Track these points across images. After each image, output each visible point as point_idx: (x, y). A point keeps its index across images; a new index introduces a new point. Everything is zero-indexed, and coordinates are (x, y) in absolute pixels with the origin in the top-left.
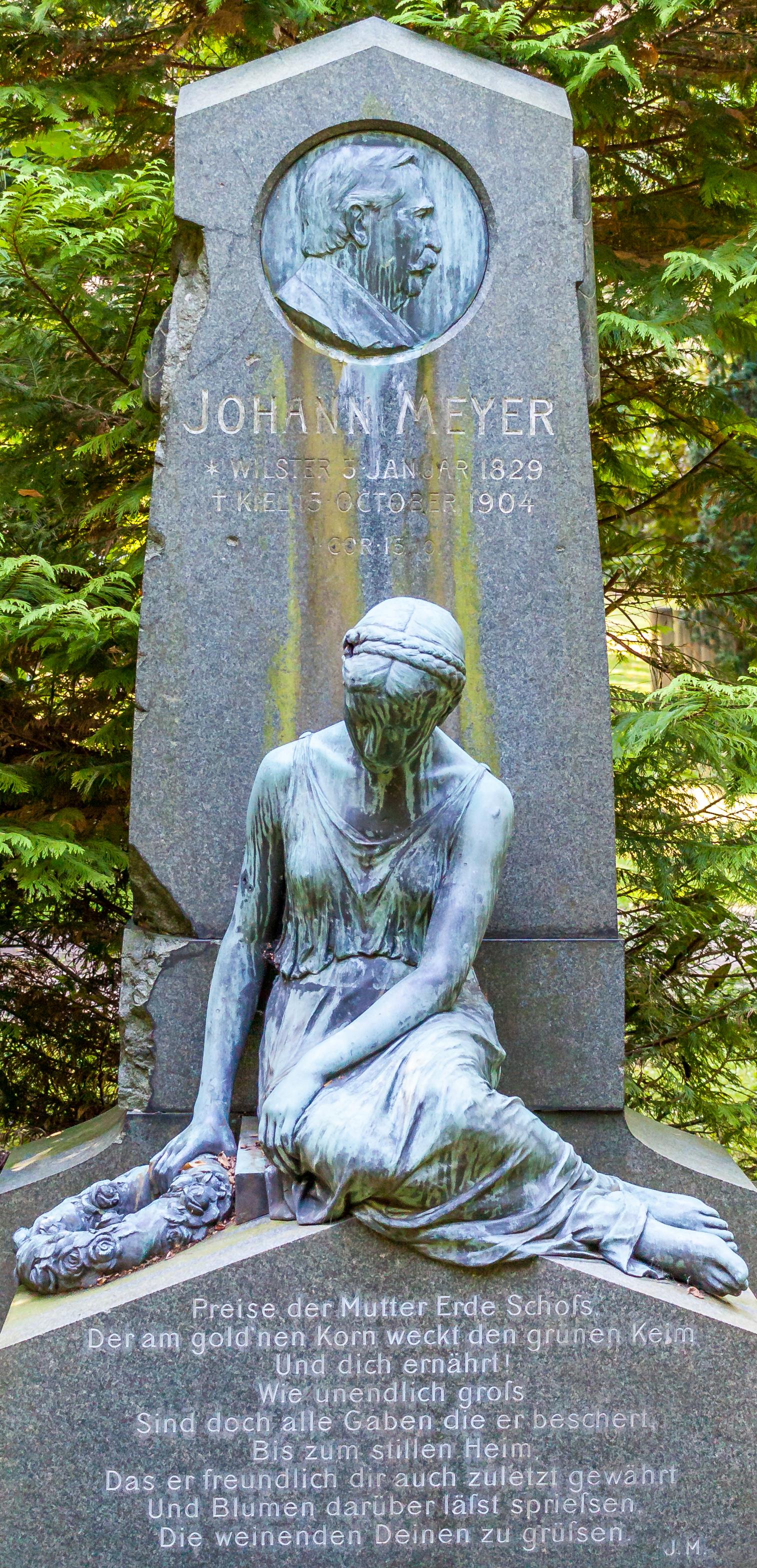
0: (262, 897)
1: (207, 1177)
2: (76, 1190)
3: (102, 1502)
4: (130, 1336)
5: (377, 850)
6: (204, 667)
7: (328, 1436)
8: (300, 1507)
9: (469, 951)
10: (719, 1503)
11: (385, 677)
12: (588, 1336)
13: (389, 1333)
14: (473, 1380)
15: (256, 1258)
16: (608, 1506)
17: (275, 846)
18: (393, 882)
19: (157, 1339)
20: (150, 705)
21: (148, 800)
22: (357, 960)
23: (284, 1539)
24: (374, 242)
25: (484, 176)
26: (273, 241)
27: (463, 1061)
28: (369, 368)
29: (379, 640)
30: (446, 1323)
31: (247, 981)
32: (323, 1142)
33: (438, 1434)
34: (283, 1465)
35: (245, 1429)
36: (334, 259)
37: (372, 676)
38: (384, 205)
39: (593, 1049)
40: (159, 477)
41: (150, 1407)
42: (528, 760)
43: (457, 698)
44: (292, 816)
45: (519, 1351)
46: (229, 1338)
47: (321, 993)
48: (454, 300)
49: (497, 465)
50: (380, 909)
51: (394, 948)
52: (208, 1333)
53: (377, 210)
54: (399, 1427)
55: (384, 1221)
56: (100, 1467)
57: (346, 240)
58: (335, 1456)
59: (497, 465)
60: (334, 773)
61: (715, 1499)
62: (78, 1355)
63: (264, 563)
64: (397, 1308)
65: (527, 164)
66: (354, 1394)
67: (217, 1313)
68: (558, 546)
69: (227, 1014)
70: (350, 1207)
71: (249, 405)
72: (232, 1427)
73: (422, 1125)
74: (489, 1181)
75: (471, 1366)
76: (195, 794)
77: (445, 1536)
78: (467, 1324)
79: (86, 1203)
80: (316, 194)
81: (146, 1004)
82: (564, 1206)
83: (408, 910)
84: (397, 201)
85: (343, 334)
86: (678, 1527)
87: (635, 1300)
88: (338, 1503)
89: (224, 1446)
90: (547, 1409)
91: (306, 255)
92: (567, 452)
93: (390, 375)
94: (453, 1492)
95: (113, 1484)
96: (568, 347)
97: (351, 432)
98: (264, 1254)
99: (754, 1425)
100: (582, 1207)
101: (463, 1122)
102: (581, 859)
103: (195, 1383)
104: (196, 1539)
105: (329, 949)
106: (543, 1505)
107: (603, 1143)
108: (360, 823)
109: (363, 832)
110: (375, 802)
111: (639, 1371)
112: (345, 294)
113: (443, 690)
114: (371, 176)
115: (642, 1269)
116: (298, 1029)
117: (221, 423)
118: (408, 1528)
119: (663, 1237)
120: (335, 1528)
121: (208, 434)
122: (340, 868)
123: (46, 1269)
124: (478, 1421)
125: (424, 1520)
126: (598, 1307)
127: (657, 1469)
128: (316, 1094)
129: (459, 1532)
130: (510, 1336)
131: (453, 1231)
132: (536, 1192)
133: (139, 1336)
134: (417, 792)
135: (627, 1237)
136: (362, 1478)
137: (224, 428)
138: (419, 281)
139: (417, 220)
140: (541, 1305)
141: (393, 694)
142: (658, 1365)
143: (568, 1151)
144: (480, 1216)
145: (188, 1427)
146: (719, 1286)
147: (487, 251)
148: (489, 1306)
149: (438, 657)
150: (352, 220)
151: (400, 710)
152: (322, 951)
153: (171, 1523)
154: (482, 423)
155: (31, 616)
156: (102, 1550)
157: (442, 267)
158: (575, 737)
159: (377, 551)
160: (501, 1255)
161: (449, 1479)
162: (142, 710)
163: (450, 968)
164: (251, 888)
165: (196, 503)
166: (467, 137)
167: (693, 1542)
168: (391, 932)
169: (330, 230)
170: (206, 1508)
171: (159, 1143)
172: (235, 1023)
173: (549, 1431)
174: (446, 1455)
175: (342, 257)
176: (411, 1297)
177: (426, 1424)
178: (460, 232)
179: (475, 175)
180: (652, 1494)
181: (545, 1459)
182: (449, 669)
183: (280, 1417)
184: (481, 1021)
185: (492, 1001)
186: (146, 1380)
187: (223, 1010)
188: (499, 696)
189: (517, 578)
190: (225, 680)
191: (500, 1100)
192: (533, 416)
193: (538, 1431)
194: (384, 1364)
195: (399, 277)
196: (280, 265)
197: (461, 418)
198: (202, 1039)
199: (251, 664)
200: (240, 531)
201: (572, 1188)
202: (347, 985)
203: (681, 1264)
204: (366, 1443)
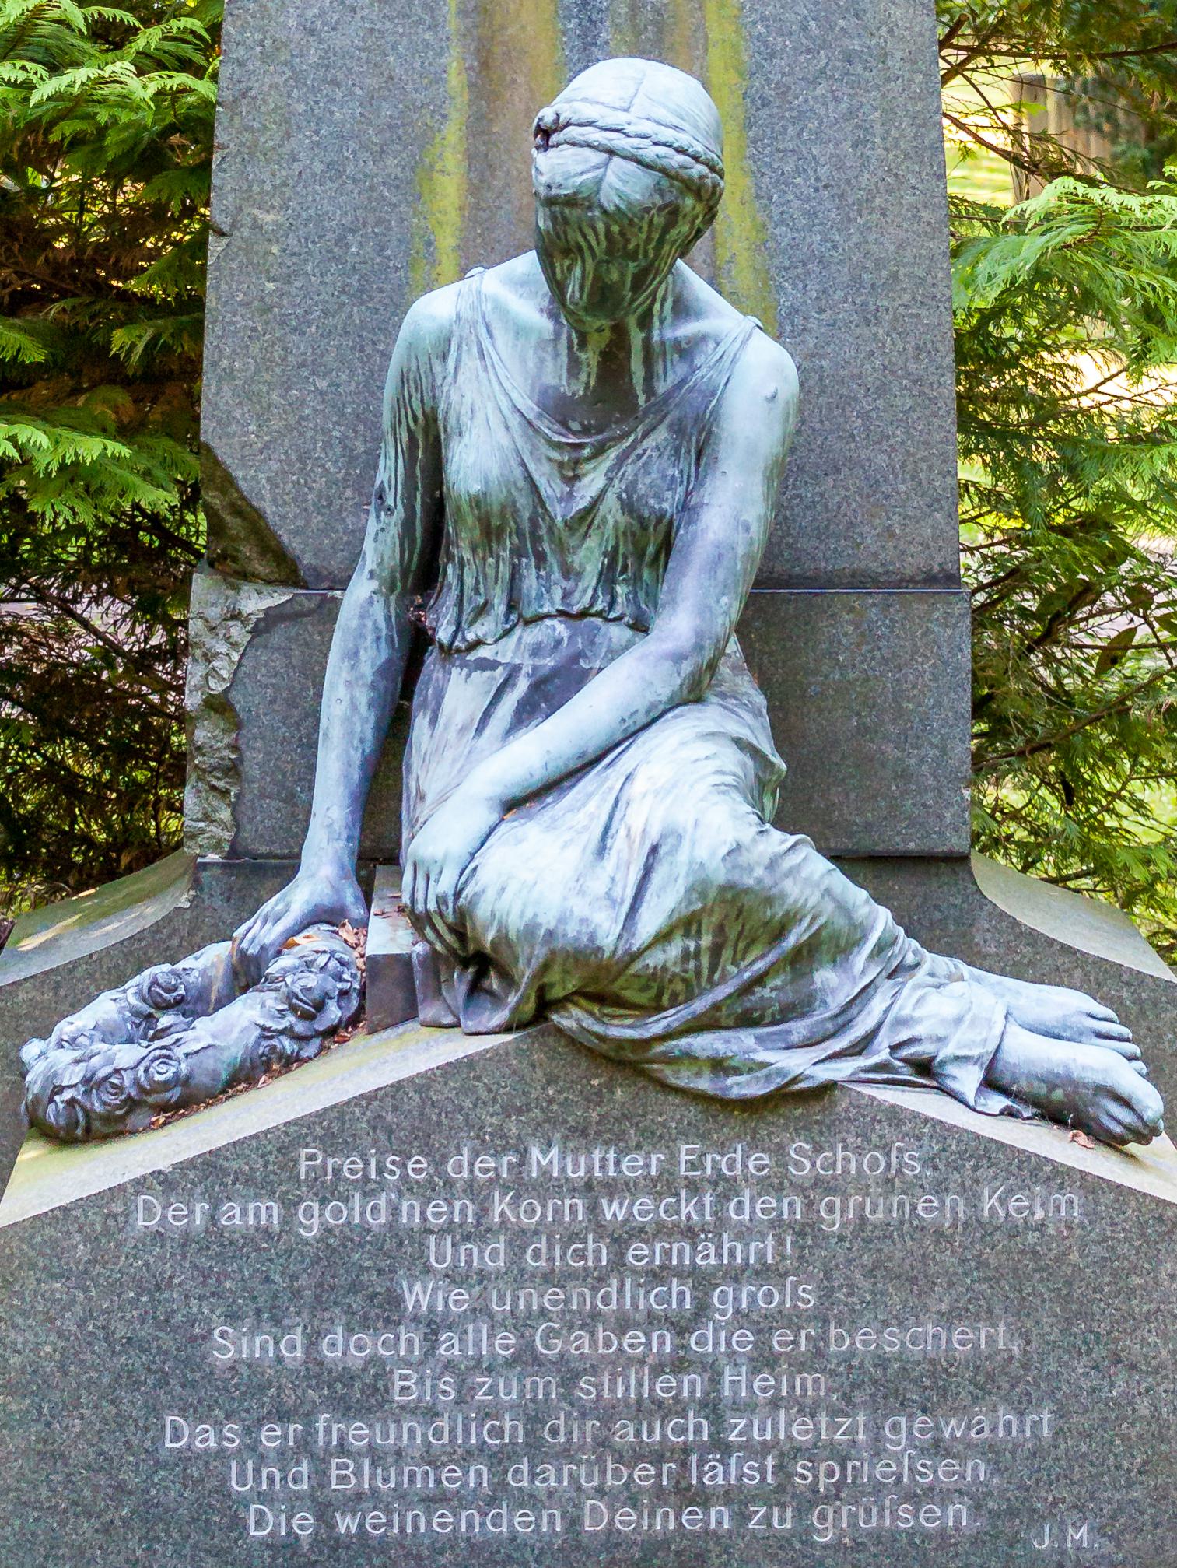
0: (408, 525)
1: (322, 960)
2: (118, 981)
3: (159, 1465)
4: (202, 1207)
5: (587, 452)
7: (510, 1363)
9: (729, 608)
10: (1118, 1467)
11: (599, 182)
12: (914, 1207)
13: (604, 1202)
14: (735, 1276)
15: (398, 1086)
16: (944, 1472)
17: (428, 445)
18: (611, 500)
20: (233, 225)
21: (230, 373)
22: (555, 622)
23: (442, 1522)
29: (589, 124)
30: (694, 1187)
31: (385, 654)
32: (502, 906)
33: (682, 1359)
34: (439, 1408)
35: (381, 1351)
37: (579, 180)
41: (233, 1317)
42: (822, 311)
43: (711, 215)
45: (807, 1230)
46: (355, 1211)
47: (500, 674)
50: (591, 543)
51: (612, 604)
52: (323, 1202)
54: (620, 1349)
55: (598, 1028)
56: (155, 1410)
58: (521, 1394)
60: (520, 331)
61: (1111, 1461)
62: (121, 1236)
64: (618, 1163)
67: (337, 1171)
69: (354, 706)
70: (545, 1006)
72: (360, 1348)
76: (303, 365)
77: (691, 1519)
78: (726, 1188)
79: (134, 1001)
81: (227, 691)
82: (877, 1005)
83: (635, 544)
86: (1054, 1504)
87: (987, 1151)
88: (525, 1467)
89: (348, 1377)
90: (851, 1321)
95: (176, 1438)
100: (905, 1005)
101: (720, 876)
102: (903, 465)
104: (304, 1524)
105: (512, 606)
106: (844, 1469)
107: (937, 907)
108: (559, 409)
109: (564, 424)
110: (583, 377)
111: (993, 1262)
113: (689, 201)
116: (463, 730)
118: (634, 1506)
119: (1031, 1054)
120: (521, 1506)
122: (529, 479)
123: (72, 1103)
124: (744, 1340)
125: (659, 1494)
126: (930, 1162)
127: (1021, 1414)
128: (492, 831)
129: (713, 1511)
130: (793, 1207)
131: (704, 1043)
132: (833, 984)
133: (216, 1207)
134: (648, 362)
135: (975, 1052)
140: (842, 1159)
141: (611, 208)
142: (1022, 1252)
143: (882, 919)
144: (746, 1021)
145: (293, 1349)
146: (1118, 1130)
148: (760, 1161)
149: (681, 151)
151: (622, 233)
152: (500, 608)
155: (48, 87)
156: (158, 1540)
158: (895, 276)
161: (698, 1429)
163: (699, 635)
167: (1077, 1528)
168: (607, 578)
170: (321, 1474)
171: (247, 907)
172: (365, 721)
173: (853, 1355)
174: (693, 1392)
176: (638, 1147)
177: (662, 1344)
180: (1013, 1453)
181: (847, 1398)
182: (699, 169)
183: (435, 1333)
184: (748, 717)
186: (227, 1276)
187: (346, 702)
188: (776, 212)
189: (805, 28)
190: (350, 186)
191: (777, 840)
193: (837, 1355)
199: (390, 161)
201: (890, 977)
202: (540, 662)
203: (1058, 1095)
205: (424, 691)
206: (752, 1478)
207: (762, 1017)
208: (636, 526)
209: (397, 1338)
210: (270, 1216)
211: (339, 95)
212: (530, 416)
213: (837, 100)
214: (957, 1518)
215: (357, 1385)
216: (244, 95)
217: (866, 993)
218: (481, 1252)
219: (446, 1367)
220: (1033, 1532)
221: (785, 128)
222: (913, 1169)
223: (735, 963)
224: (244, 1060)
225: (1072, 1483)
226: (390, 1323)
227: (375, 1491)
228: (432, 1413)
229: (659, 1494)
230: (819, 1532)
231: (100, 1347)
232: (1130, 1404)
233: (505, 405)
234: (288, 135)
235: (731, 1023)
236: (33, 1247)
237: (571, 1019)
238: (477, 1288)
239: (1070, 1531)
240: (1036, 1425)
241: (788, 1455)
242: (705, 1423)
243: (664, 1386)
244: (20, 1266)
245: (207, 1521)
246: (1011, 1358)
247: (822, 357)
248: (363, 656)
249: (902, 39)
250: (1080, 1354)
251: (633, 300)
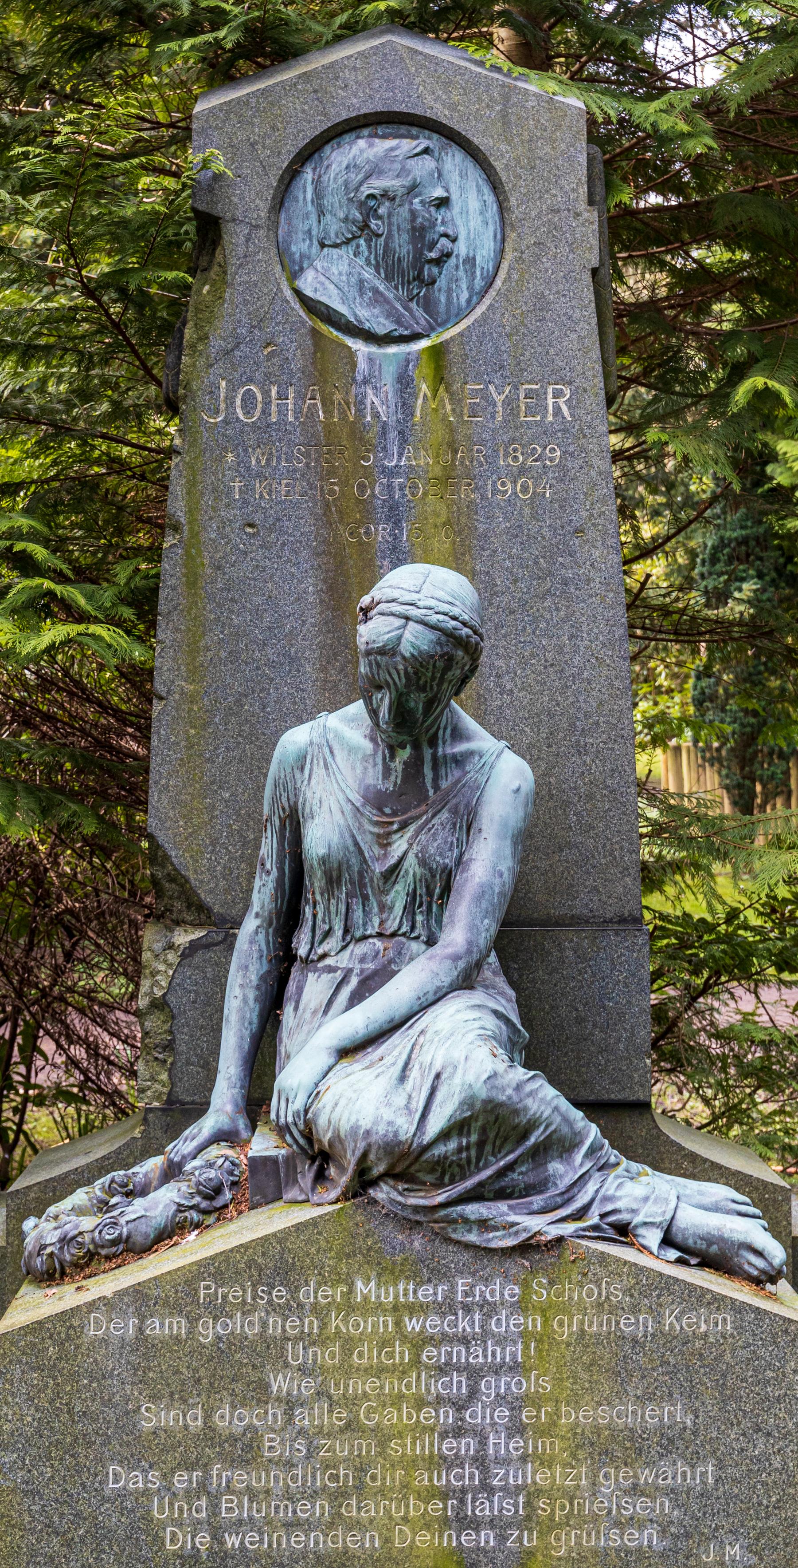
0: (280, 882)
1: (220, 1162)
2: (89, 1182)
3: (105, 1500)
4: (134, 1321)
5: (395, 827)
6: (223, 654)
7: (342, 1431)
8: (313, 1507)
9: (488, 928)
10: (760, 1504)
11: (399, 638)
12: (618, 1323)
13: (407, 1319)
14: (496, 1370)
15: (265, 1239)
16: (640, 1507)
17: (293, 825)
18: (411, 859)
19: (162, 1325)
20: (168, 692)
21: (166, 787)
22: (375, 940)
24: (390, 231)
25: (498, 165)
26: (289, 233)
27: (482, 1032)
28: (385, 355)
29: (393, 601)
30: (468, 1309)
31: (265, 967)
32: (335, 1116)
33: (460, 1428)
34: (295, 1461)
35: (255, 1421)
36: (351, 250)
37: (387, 637)
38: (399, 193)
39: (619, 1041)
40: (177, 465)
41: (154, 1398)
42: (549, 746)
44: (309, 795)
45: (544, 1340)
46: (237, 1323)
47: (339, 975)
48: (470, 288)
49: (515, 450)
50: (398, 887)
51: (413, 927)
52: (216, 1318)
53: (393, 199)
54: (418, 1421)
55: (400, 1199)
56: (100, 1461)
57: (362, 230)
58: (351, 1452)
59: (515, 450)
60: (352, 750)
61: (755, 1500)
62: (79, 1342)
63: (282, 549)
64: (415, 1292)
65: (541, 153)
66: (369, 1386)
67: (224, 1297)
68: (577, 531)
69: (245, 1000)
71: (266, 393)
72: (241, 1419)
73: (439, 1096)
74: (511, 1157)
75: (494, 1354)
76: (213, 782)
77: (467, 1539)
78: (489, 1309)
79: (99, 1193)
80: (332, 185)
81: (164, 995)
82: (591, 1187)
83: (427, 887)
84: (413, 189)
85: (359, 321)
86: (716, 1529)
88: (354, 1503)
89: (233, 1439)
91: (323, 246)
92: (585, 436)
93: (408, 362)
94: (475, 1491)
95: (116, 1481)
96: (584, 333)
97: (369, 419)
98: (274, 1235)
99: (795, 1420)
100: (610, 1188)
101: (483, 1094)
102: (604, 846)
103: (202, 1372)
105: (346, 931)
106: (571, 1504)
107: (631, 1138)
108: (377, 800)
109: (380, 810)
110: (393, 778)
111: (672, 1361)
112: (361, 282)
113: (460, 653)
114: (386, 166)
115: (673, 1254)
116: (315, 1012)
117: (239, 411)
118: (428, 1530)
119: (695, 1220)
120: (350, 1530)
121: (226, 422)
122: (356, 844)
123: (51, 1255)
124: (503, 1414)
125: (445, 1522)
126: (628, 1292)
127: (693, 1466)
128: (330, 1069)
129: (483, 1533)
131: (473, 1210)
133: (142, 1321)
134: (435, 768)
135: (658, 1220)
136: (382, 1476)
137: (242, 417)
138: (435, 270)
139: (432, 209)
141: (407, 655)
142: (692, 1354)
143: (593, 1131)
144: (502, 1195)
146: (756, 1273)
147: (503, 240)
149: (454, 618)
150: (369, 207)
151: (416, 673)
152: (339, 932)
153: (180, 1524)
154: (500, 409)
156: (103, 1551)
157: (457, 256)
158: (597, 723)
159: (396, 537)
160: (524, 1236)
161: (472, 1478)
162: (161, 698)
163: (470, 943)
164: (268, 873)
165: (215, 490)
166: (482, 127)
167: (733, 1547)
168: (410, 910)
169: (346, 220)
170: (214, 1507)
171: (174, 1132)
172: (252, 1010)
173: (577, 1425)
174: (467, 1450)
175: (358, 246)
176: (429, 1281)
177: (447, 1417)
178: (475, 222)
179: (490, 165)
180: (688, 1493)
181: (574, 1456)
182: (466, 631)
183: (291, 1409)
184: (503, 1001)
185: (512, 983)
186: (150, 1369)
187: (240, 997)
188: (519, 683)
189: (536, 563)
190: (243, 667)
191: (520, 1073)
192: (550, 401)
193: (565, 1425)
194: (402, 1353)
195: (416, 264)
196: (297, 256)
197: (478, 404)
198: (220, 1030)
199: (270, 651)
200: (258, 518)
201: (599, 1170)
202: (366, 966)
203: (714, 1249)
204: (382, 1437)
205: (292, 987)
206: (509, 1510)
207: (513, 1193)
208: (428, 876)
209: (266, 1413)
210: (179, 1328)
211: (236, 608)
212: (358, 804)
213: (557, 609)
214: (650, 1540)
215: (239, 1445)
216: (175, 609)
217: (583, 1179)
218: (323, 1353)
219: (299, 1433)
220: (702, 1549)
221: (525, 628)
222: (617, 1296)
223: (494, 1155)
224: (166, 1226)
225: (729, 1515)
226: (262, 1402)
227: (251, 1518)
228: (290, 1464)
229: (445, 1522)
230: (555, 1548)
231: (65, 1417)
232: (768, 1460)
233: (341, 797)
234: (204, 634)
235: (491, 1195)
236: (18, 1348)
237: (382, 1193)
238: (320, 1379)
239: (728, 1548)
240: (703, 1474)
241: (533, 1494)
242: (477, 1472)
243: (447, 1447)
244: (11, 1362)
245: (137, 1539)
246: (685, 1428)
247: (550, 776)
248: (251, 968)
249: (600, 570)
250: (732, 1425)
251: (424, 722)
